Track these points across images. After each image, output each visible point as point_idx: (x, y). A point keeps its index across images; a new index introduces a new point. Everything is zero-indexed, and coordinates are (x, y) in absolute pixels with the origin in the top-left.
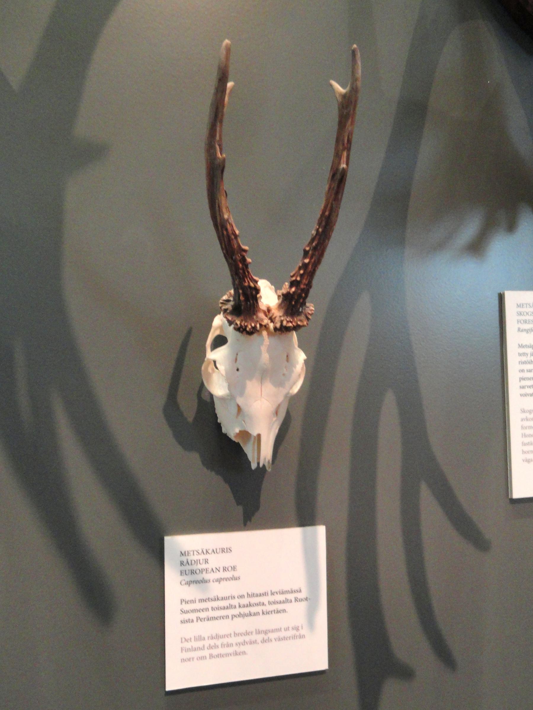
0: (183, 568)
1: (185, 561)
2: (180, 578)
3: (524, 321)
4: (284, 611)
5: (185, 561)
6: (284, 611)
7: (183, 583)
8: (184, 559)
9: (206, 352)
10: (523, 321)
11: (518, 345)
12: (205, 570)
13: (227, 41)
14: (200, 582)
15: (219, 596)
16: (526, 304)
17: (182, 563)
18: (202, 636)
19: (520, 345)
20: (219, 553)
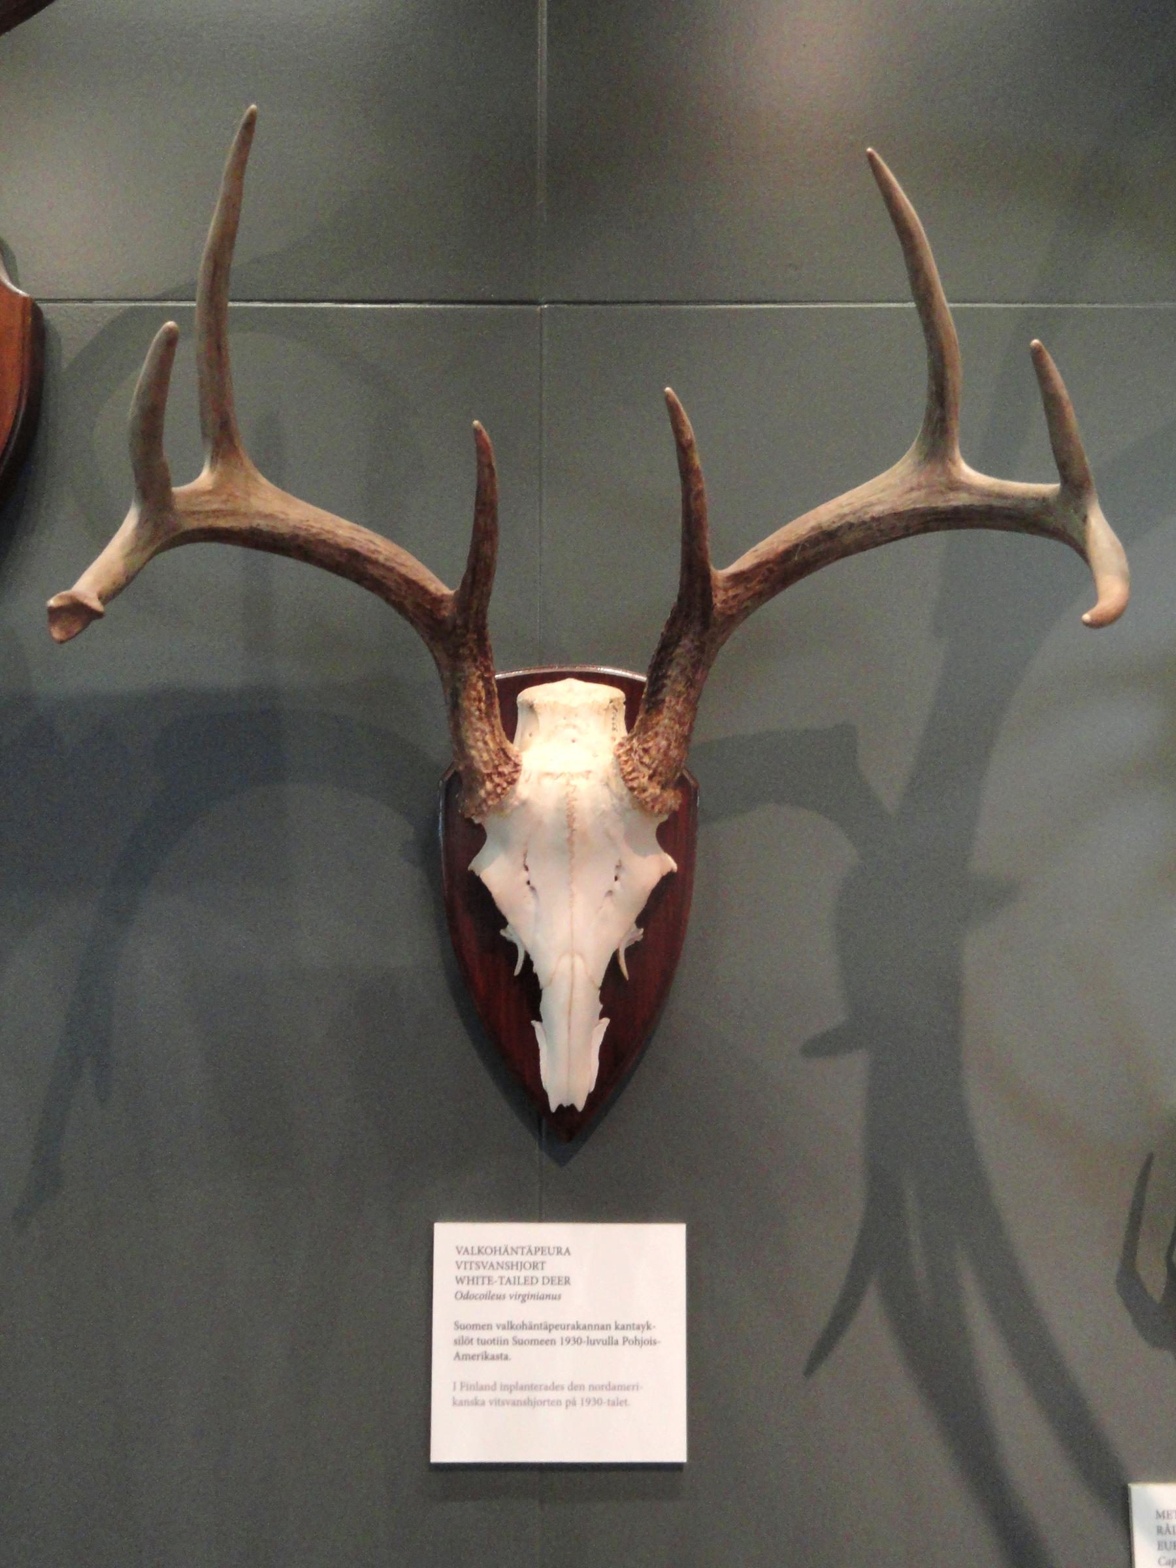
0: (1161, 1538)
1: (1164, 1527)
2: (1159, 1554)
3: (532, 1266)
4: (624, 1402)
5: (1164, 1527)
6: (624, 1402)
7: (1163, 1561)
8: (1163, 1523)
9: (540, 1015)
10: (529, 1266)
11: (1156, 1513)
12: (541, 1249)
13: (253, 106)
14: (527, 1248)
15: (618, 1322)
16: (472, 1254)
17: (1159, 1530)
18: (615, 1339)
19: (1160, 1511)
20: (553, 1254)
